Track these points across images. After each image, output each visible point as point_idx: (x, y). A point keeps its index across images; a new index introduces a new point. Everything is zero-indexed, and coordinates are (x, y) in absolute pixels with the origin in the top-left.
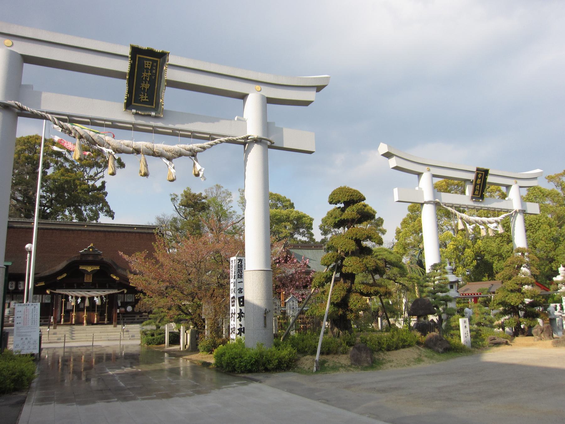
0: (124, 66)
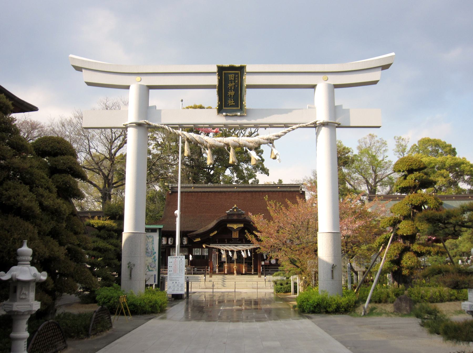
0: (214, 80)
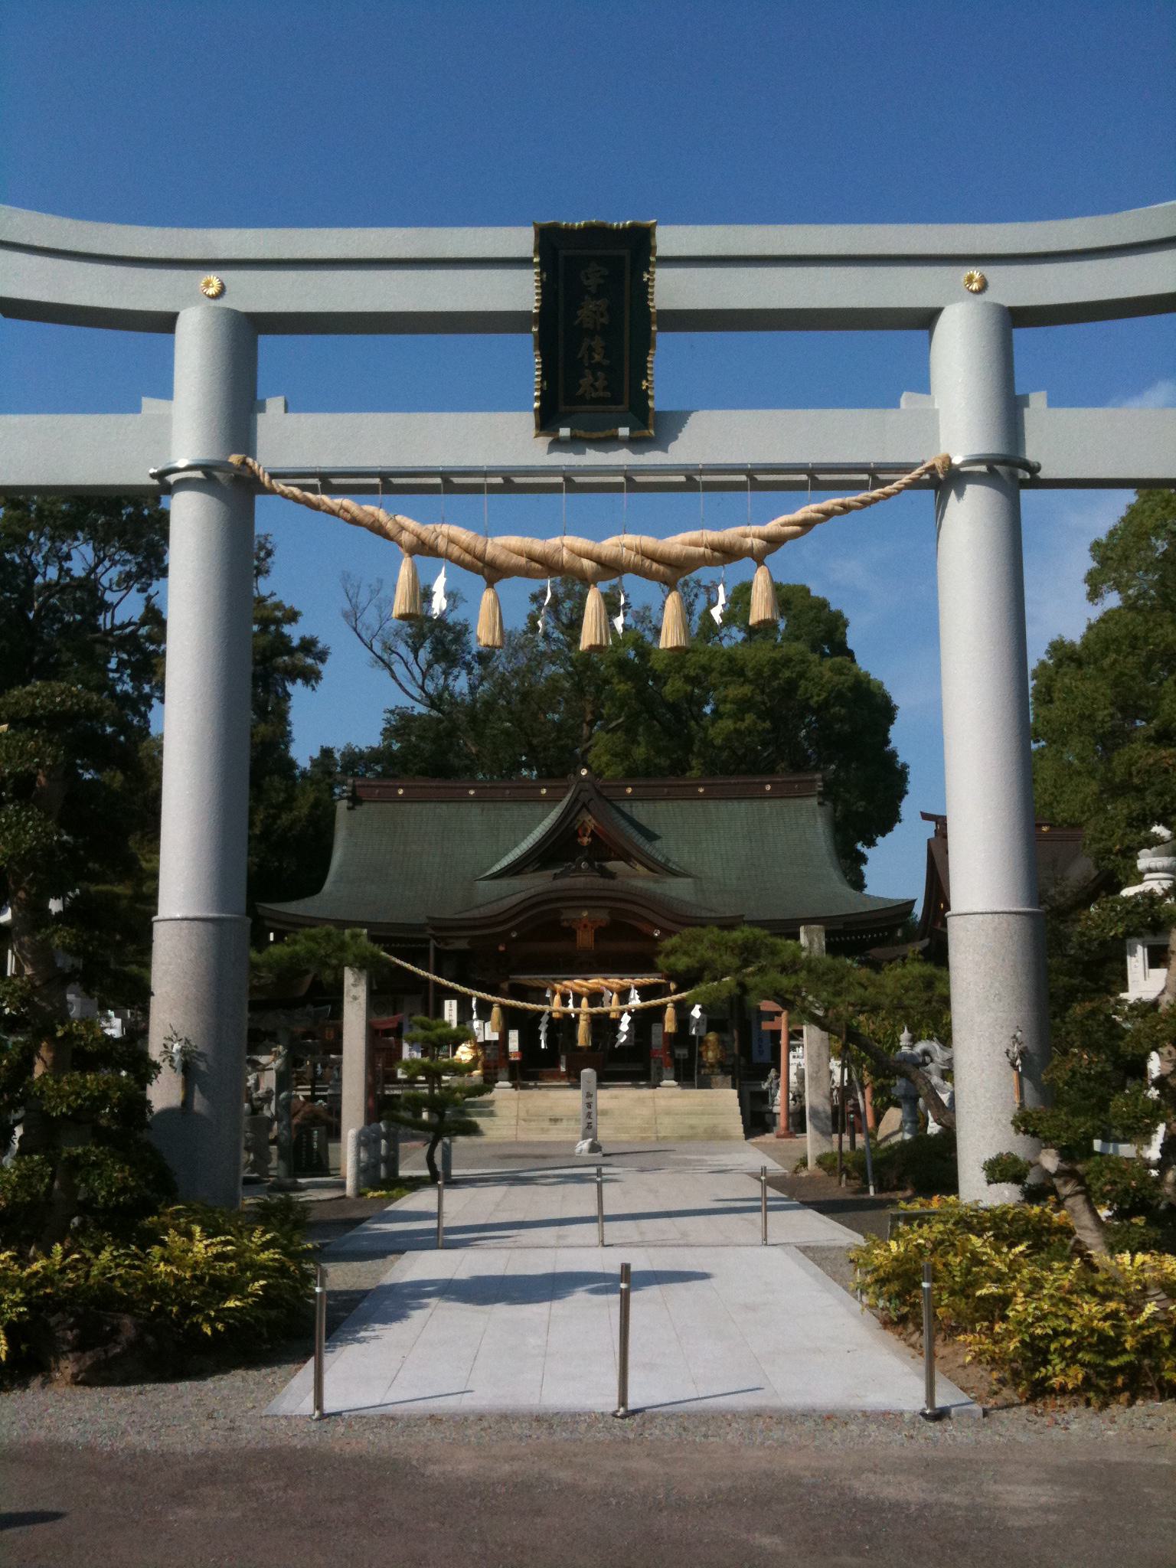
0: (520, 291)
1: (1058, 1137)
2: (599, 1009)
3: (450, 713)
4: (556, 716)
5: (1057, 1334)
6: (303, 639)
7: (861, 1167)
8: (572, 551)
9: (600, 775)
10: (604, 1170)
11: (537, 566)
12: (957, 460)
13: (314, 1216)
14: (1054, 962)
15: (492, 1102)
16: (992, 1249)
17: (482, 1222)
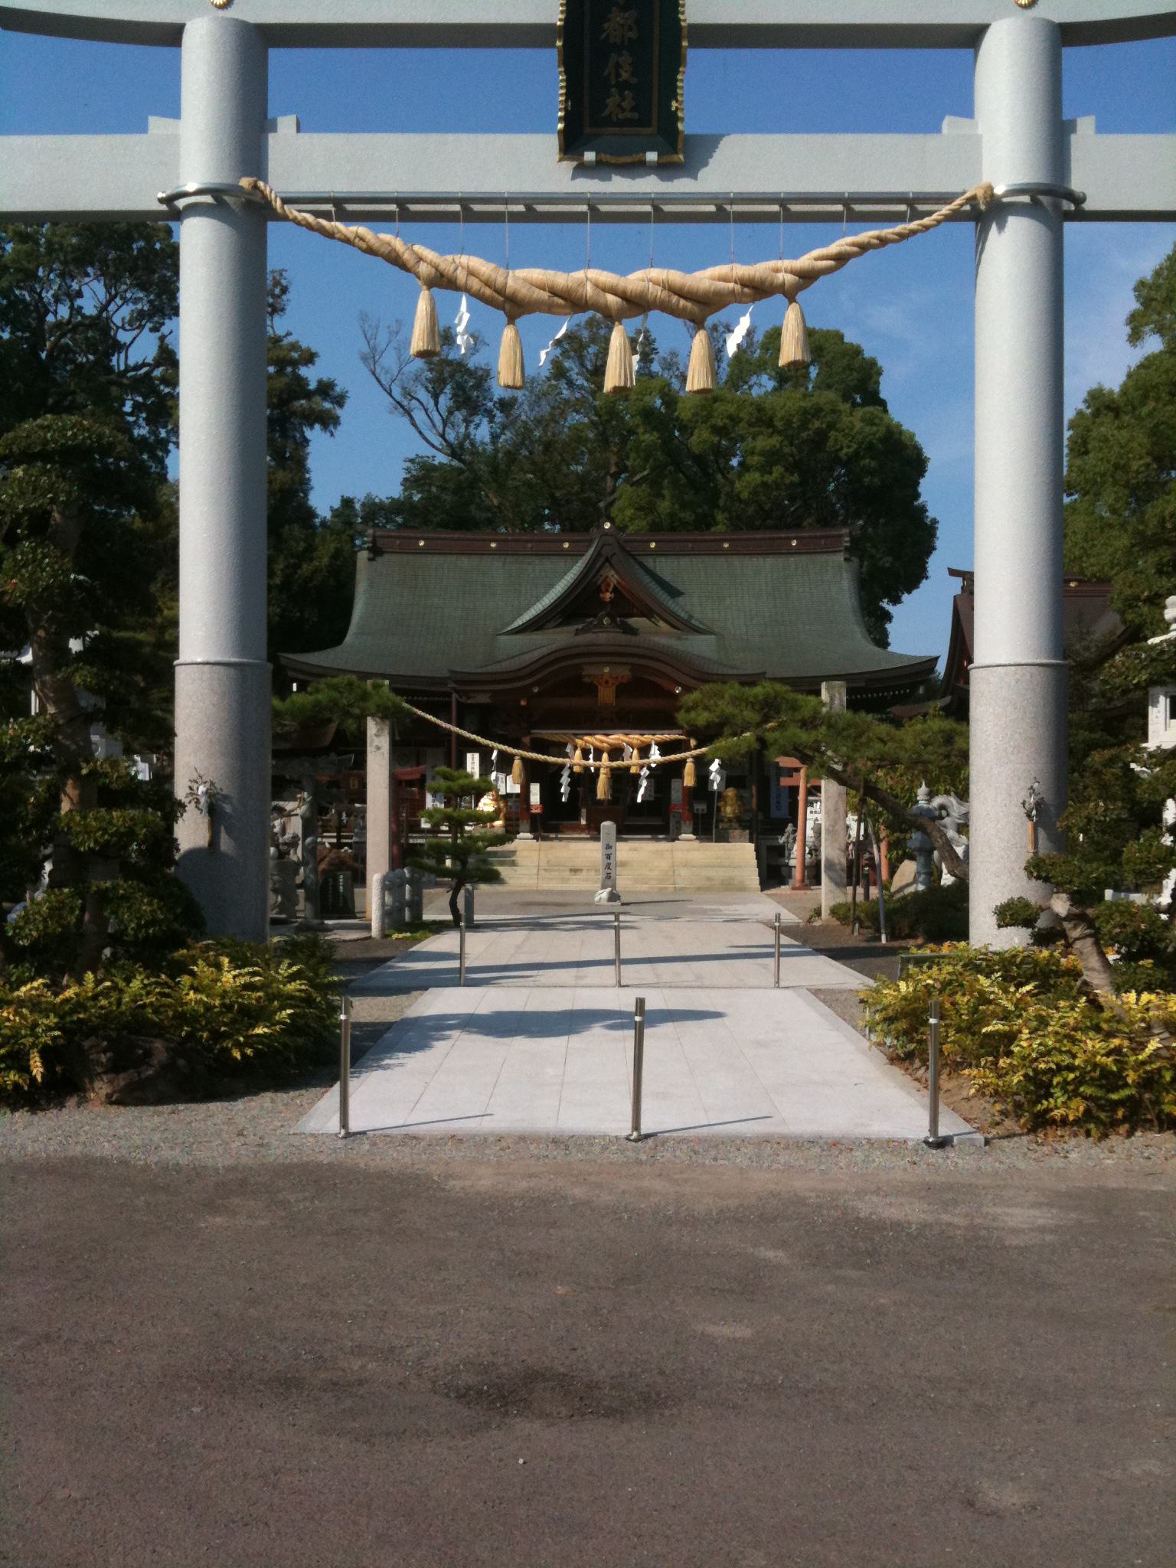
1: (1070, 882)
2: (619, 763)
3: (470, 463)
4: (580, 468)
5: (1060, 1068)
6: (320, 382)
7: (874, 917)
8: (596, 285)
9: (622, 529)
10: (622, 918)
11: (560, 301)
12: (999, 190)
13: (340, 954)
14: (1074, 717)
15: (513, 853)
16: (1000, 988)
17: (503, 963)
